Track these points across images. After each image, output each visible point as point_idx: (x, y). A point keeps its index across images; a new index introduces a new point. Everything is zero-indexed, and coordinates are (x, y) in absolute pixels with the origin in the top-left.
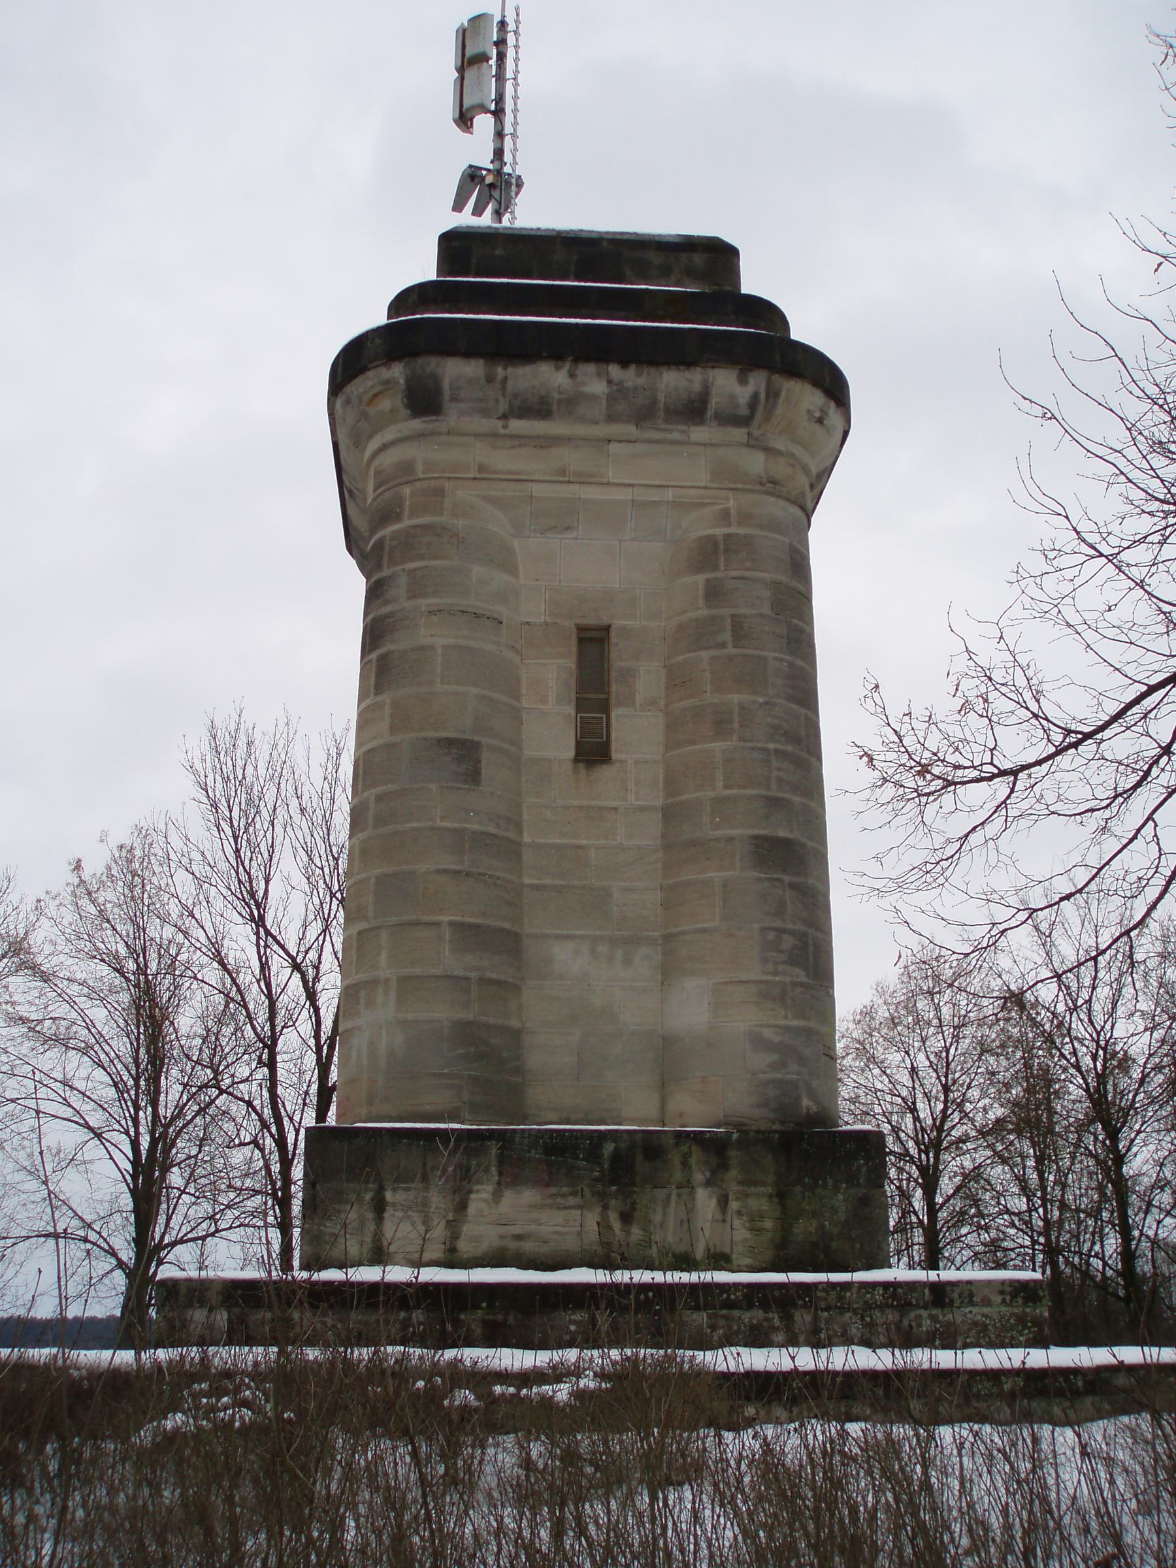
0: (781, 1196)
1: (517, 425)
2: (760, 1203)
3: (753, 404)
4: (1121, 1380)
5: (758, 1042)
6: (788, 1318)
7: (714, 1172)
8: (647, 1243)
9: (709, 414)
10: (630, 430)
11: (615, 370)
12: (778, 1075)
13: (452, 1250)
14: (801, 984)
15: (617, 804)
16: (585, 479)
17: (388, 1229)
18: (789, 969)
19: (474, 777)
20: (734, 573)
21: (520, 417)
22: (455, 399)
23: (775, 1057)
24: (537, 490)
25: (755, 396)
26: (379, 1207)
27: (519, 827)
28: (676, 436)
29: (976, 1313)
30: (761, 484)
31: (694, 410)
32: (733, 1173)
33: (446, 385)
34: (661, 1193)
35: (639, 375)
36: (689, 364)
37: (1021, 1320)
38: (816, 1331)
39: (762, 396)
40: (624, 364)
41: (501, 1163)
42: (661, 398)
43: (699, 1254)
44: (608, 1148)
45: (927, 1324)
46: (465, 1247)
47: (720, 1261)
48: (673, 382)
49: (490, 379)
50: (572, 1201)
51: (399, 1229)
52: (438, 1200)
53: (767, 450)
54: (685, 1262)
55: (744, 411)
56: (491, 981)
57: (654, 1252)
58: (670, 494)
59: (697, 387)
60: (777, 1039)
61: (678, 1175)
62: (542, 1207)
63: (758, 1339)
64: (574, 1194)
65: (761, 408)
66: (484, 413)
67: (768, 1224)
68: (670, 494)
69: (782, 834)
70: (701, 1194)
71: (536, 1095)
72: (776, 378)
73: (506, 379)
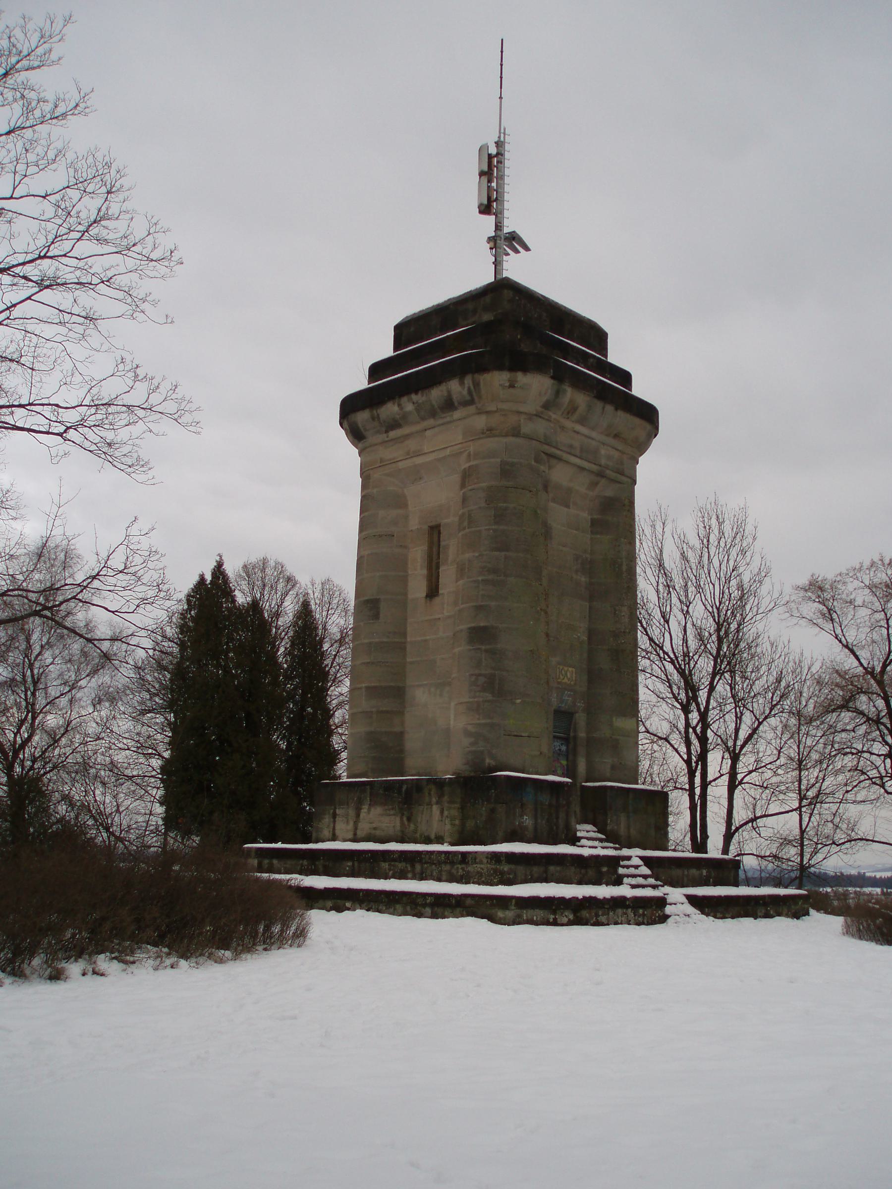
0: (462, 808)
1: (393, 434)
2: (455, 813)
3: (470, 392)
4: (469, 902)
5: (467, 733)
6: (413, 866)
7: (439, 797)
8: (415, 831)
9: (456, 404)
10: (431, 422)
11: (414, 397)
12: (473, 749)
13: (355, 834)
14: (488, 701)
15: (440, 616)
16: (418, 454)
17: (338, 827)
18: (482, 694)
19: (376, 616)
20: (470, 488)
21: (392, 430)
22: (366, 430)
23: (472, 740)
24: (401, 465)
25: (469, 389)
26: (334, 816)
27: (404, 635)
28: (448, 419)
29: (478, 867)
30: (483, 433)
31: (449, 405)
32: (446, 798)
33: (360, 425)
34: (421, 808)
35: (422, 396)
36: (440, 383)
37: (495, 871)
38: (422, 873)
39: (472, 388)
40: (416, 393)
41: (371, 794)
42: (434, 403)
43: (433, 836)
44: (405, 787)
45: (461, 872)
46: (360, 834)
47: (440, 840)
48: (436, 394)
49: (373, 419)
50: (392, 812)
51: (342, 827)
52: (352, 812)
53: (488, 413)
54: (428, 841)
55: (468, 398)
56: (382, 712)
57: (418, 835)
58: (448, 452)
59: (445, 394)
60: (473, 730)
61: (427, 799)
62: (382, 815)
63: (402, 876)
64: (393, 809)
65: (474, 394)
66: (378, 432)
67: (457, 822)
68: (448, 452)
69: (482, 624)
70: (435, 807)
71: (411, 762)
72: (476, 376)
73: (378, 415)
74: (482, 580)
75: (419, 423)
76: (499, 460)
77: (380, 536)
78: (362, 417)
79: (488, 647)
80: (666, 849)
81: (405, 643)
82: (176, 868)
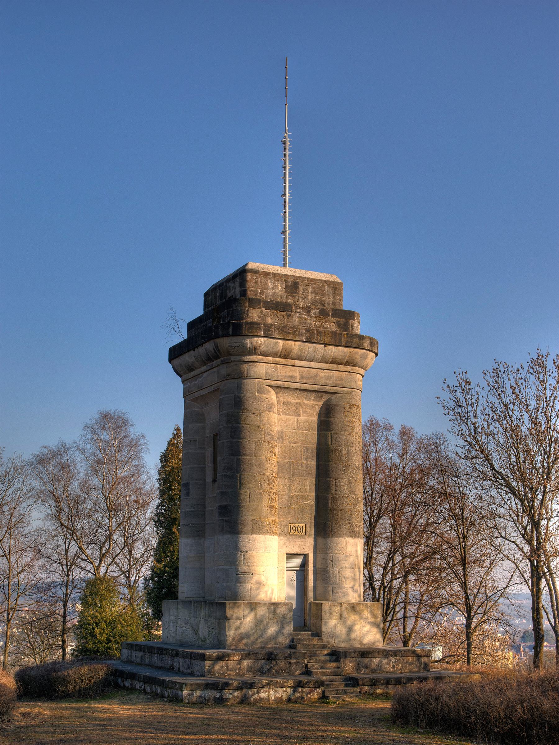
69: (224, 504)
74: (225, 475)
75: (200, 368)
76: (233, 395)
77: (190, 441)
78: (188, 358)
79: (227, 518)
80: (224, 648)
81: (204, 511)
82: (499, 635)
